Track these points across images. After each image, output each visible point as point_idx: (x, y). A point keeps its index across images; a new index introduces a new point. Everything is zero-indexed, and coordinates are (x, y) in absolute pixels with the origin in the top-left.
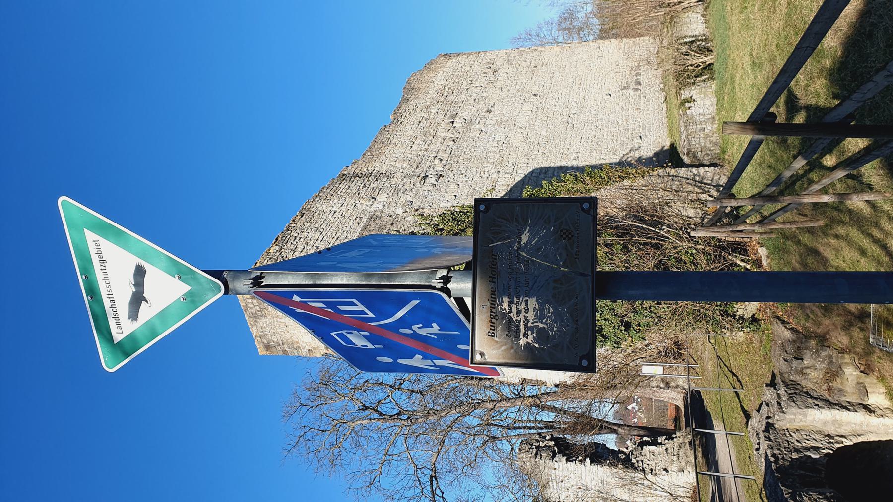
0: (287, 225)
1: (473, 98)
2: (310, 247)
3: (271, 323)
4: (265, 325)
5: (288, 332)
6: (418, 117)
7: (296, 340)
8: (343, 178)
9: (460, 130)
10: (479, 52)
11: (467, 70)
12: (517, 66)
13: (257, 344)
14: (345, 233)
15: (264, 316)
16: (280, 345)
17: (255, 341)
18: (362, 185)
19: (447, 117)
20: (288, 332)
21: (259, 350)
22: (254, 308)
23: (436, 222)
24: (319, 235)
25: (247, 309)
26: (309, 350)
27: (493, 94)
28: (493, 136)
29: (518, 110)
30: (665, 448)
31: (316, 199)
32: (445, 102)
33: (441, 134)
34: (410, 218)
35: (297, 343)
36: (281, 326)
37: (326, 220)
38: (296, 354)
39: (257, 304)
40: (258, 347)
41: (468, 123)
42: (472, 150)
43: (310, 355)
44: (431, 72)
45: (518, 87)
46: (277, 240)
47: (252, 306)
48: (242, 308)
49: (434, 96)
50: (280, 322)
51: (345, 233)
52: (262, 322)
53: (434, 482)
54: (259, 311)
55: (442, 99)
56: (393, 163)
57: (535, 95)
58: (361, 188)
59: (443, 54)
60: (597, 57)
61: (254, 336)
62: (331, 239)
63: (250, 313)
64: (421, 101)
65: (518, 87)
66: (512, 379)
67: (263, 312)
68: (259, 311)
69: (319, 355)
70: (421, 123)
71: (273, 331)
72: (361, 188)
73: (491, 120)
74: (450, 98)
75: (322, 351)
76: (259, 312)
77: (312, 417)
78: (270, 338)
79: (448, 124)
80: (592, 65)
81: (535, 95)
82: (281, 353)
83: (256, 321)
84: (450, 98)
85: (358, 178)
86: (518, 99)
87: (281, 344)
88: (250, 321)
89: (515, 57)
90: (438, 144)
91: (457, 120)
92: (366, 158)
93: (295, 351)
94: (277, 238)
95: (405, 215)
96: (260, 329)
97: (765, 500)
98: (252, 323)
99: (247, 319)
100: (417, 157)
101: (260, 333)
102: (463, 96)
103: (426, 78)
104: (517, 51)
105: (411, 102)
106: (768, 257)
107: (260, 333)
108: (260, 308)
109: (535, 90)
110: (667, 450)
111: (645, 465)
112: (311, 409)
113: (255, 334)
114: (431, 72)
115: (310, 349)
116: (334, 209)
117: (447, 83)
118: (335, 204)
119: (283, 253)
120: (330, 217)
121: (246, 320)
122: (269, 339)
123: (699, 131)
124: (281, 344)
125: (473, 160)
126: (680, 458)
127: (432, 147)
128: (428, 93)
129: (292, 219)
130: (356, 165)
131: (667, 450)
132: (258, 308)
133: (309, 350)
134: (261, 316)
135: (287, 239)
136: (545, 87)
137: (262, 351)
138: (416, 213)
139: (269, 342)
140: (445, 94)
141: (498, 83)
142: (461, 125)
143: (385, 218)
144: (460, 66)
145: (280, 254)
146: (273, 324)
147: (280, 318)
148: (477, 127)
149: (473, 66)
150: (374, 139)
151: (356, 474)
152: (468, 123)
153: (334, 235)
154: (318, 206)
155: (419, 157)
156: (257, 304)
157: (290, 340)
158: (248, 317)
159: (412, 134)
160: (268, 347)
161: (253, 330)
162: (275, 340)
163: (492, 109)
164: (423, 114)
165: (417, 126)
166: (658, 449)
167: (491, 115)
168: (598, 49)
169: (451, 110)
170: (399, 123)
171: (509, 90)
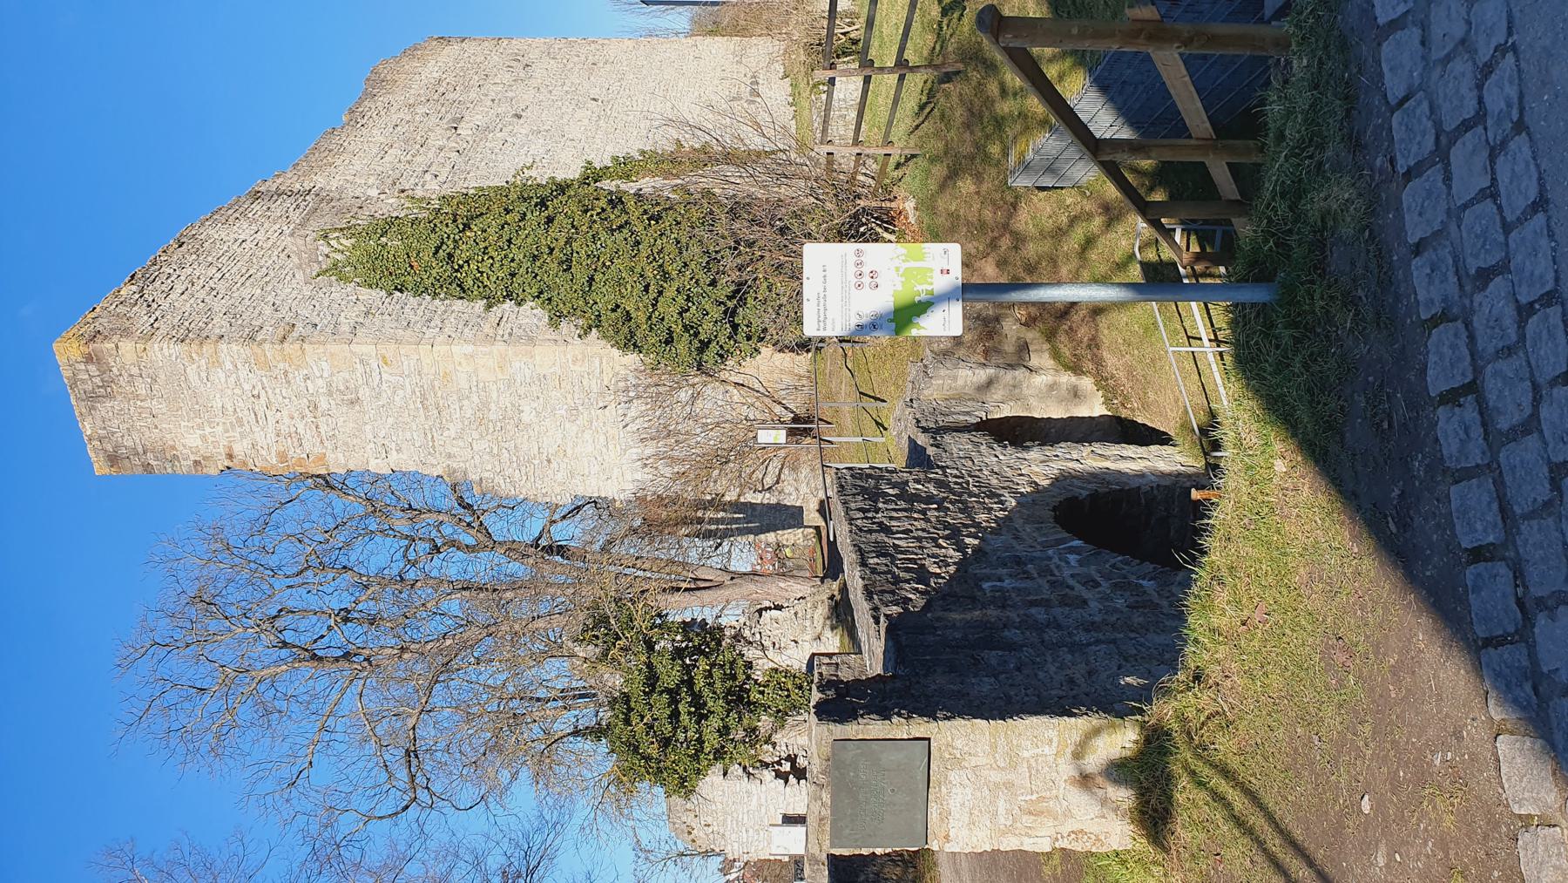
0: (152, 257)
1: (490, 98)
2: (198, 288)
3: (121, 410)
4: (111, 414)
5: (156, 427)
6: (395, 118)
7: (171, 443)
8: (256, 196)
9: (469, 139)
10: (500, 39)
11: (478, 61)
12: (565, 61)
13: (92, 454)
14: (264, 269)
15: (110, 396)
16: (138, 454)
17: (89, 446)
18: (294, 206)
19: (445, 121)
20: (156, 427)
21: (96, 466)
22: (89, 382)
23: (437, 206)
24: (214, 271)
25: (75, 383)
26: (196, 463)
27: (525, 96)
28: (525, 148)
29: (566, 117)
30: (793, 612)
31: (207, 223)
32: (442, 101)
33: (436, 140)
34: (391, 201)
35: (173, 448)
36: (143, 415)
37: (227, 251)
38: (169, 470)
39: (98, 373)
40: (94, 459)
41: (483, 130)
42: (491, 164)
43: (196, 471)
44: (416, 60)
45: (566, 88)
46: (133, 277)
47: (87, 376)
48: (66, 381)
49: (422, 92)
50: (141, 407)
51: (264, 269)
52: (104, 408)
53: (414, 762)
54: (99, 387)
55: (435, 97)
56: (350, 178)
57: (594, 99)
58: (291, 209)
59: (436, 37)
60: (692, 58)
61: (86, 438)
62: (238, 277)
63: (82, 392)
64: (398, 98)
65: (566, 88)
66: (559, 498)
67: (109, 390)
68: (99, 387)
69: (213, 471)
70: (399, 128)
71: (126, 426)
72: (291, 209)
73: (522, 129)
74: (451, 96)
75: (219, 463)
76: (102, 390)
77: (179, 665)
78: (120, 439)
79: (447, 129)
80: (684, 68)
81: (594, 99)
82: (141, 469)
83: (93, 408)
84: (451, 96)
85: (285, 197)
86: (567, 103)
87: (140, 450)
88: (79, 408)
89: (560, 49)
90: (430, 155)
91: (463, 124)
92: (299, 170)
93: (168, 465)
94: (134, 275)
95: (383, 196)
96: (99, 423)
97: (966, 877)
98: (84, 410)
99: (73, 402)
100: (393, 170)
101: (100, 431)
102: (473, 95)
103: (406, 67)
104: (564, 41)
105: (381, 99)
106: (916, 209)
107: (100, 431)
108: (102, 381)
109: (594, 93)
110: (796, 614)
111: (764, 638)
112: (176, 651)
113: (89, 433)
114: (416, 60)
115: (198, 459)
116: (242, 237)
117: (444, 76)
118: (243, 230)
119: (146, 296)
120: (235, 247)
121: (72, 406)
122: (117, 441)
123: (838, 118)
124: (140, 450)
125: (492, 177)
126: (815, 622)
127: (419, 159)
128: (411, 88)
129: (161, 250)
130: (281, 180)
131: (796, 614)
132: (97, 381)
133: (195, 462)
134: (103, 397)
135: (153, 277)
136: (610, 91)
137: (100, 467)
138: (402, 195)
139: (116, 447)
140: (441, 90)
141: (533, 81)
142: (470, 132)
143: (348, 201)
144: (466, 55)
145: (141, 297)
146: (127, 411)
147: (142, 401)
148: (498, 135)
149: (489, 58)
150: (312, 145)
151: (262, 766)
152: (483, 130)
153: (244, 271)
154: (212, 232)
155: (397, 171)
156: (98, 373)
157: (160, 443)
158: (77, 399)
159: (382, 140)
160: (113, 459)
161: (84, 426)
162: (129, 443)
163: (524, 114)
164: (402, 115)
165: (391, 130)
166: (783, 614)
167: (522, 121)
168: (694, 48)
169: (452, 111)
170: (359, 125)
171: (551, 92)
